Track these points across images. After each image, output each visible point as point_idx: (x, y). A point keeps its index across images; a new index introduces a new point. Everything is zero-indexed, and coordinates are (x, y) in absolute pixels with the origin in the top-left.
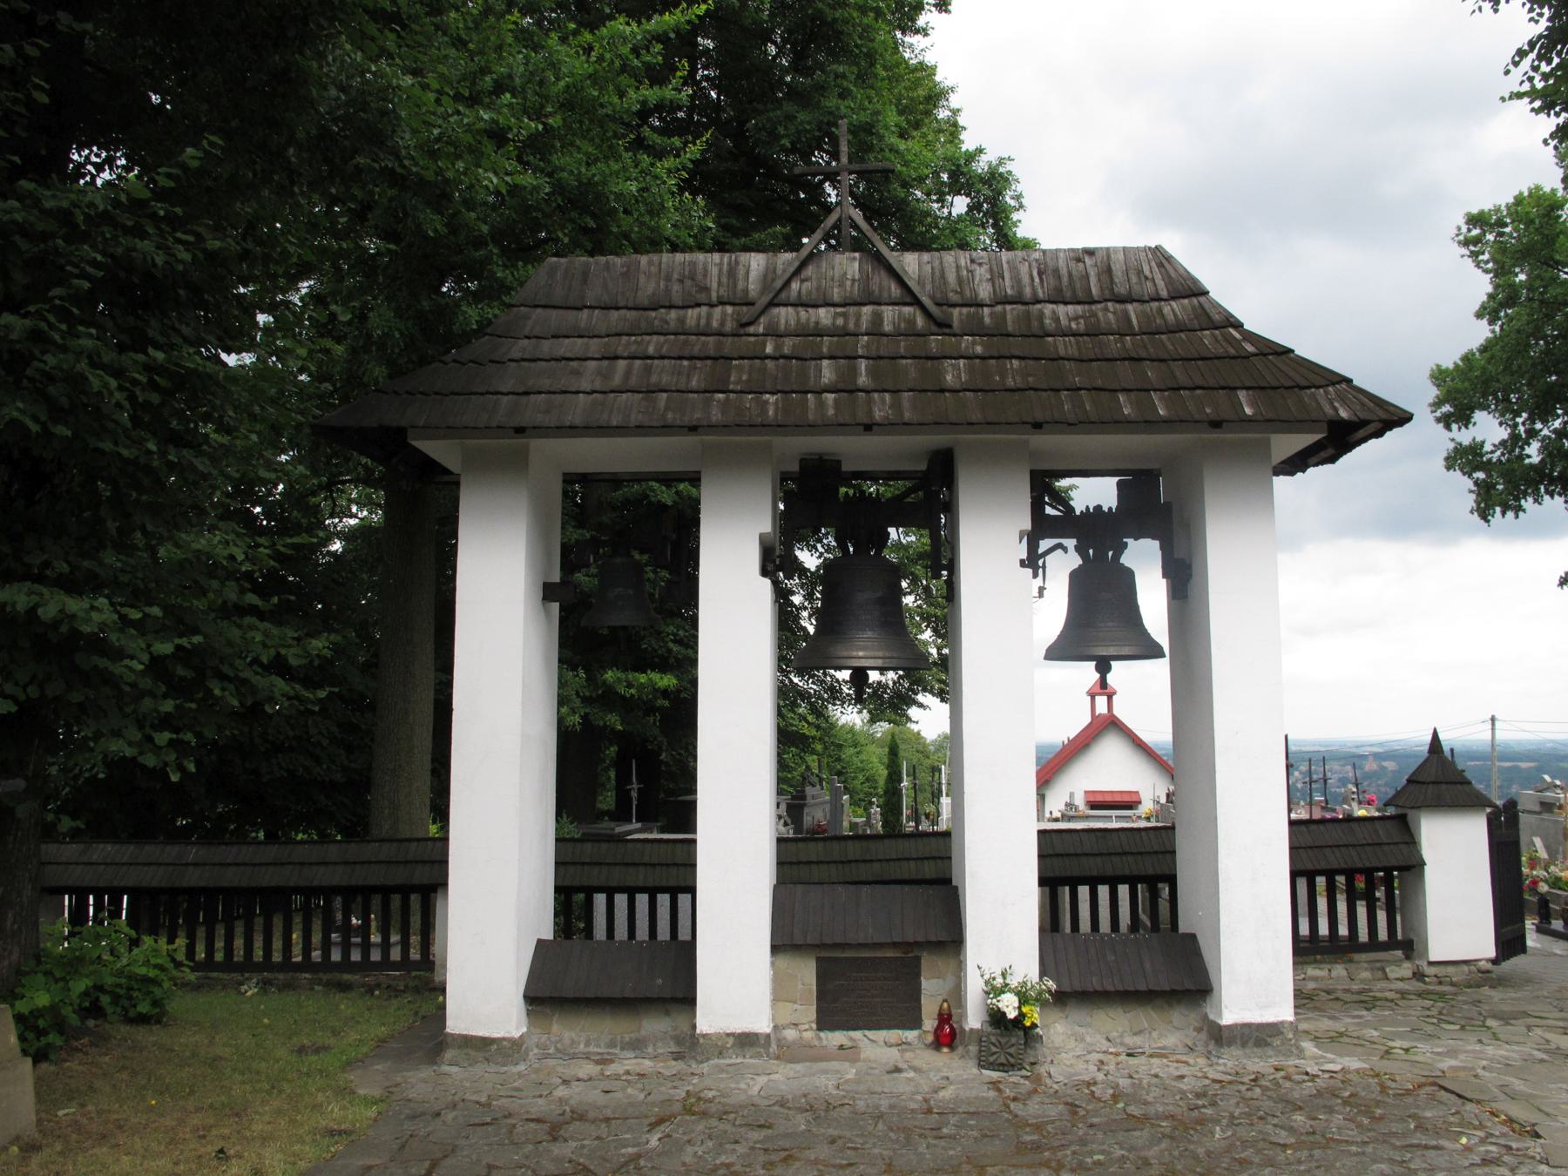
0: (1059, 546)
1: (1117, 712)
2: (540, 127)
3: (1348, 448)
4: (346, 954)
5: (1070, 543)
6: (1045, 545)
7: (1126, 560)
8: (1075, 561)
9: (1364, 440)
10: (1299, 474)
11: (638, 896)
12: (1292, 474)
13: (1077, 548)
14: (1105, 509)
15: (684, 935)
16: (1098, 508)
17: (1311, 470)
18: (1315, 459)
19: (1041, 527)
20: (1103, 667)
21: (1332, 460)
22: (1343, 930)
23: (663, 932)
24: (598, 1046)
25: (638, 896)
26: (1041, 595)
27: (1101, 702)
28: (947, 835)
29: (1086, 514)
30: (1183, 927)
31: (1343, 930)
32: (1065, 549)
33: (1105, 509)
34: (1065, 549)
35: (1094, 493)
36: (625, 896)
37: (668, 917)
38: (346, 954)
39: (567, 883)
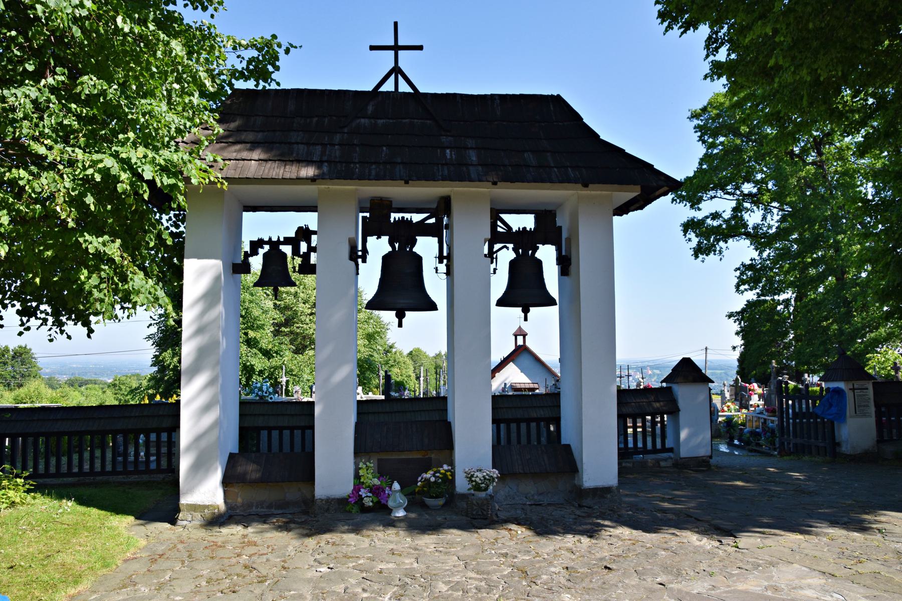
0: (505, 247)
1: (529, 344)
2: (720, 147)
3: (649, 201)
4: (158, 437)
5: (511, 246)
6: (497, 247)
7: (538, 255)
8: (512, 255)
9: (658, 197)
10: (625, 215)
11: (285, 432)
12: (621, 215)
13: (513, 249)
14: (528, 229)
15: (308, 450)
16: (524, 228)
17: (631, 213)
18: (633, 208)
19: (495, 238)
20: (526, 311)
21: (641, 208)
22: (640, 445)
23: (298, 448)
24: (262, 507)
25: (285, 432)
26: (495, 273)
27: (520, 339)
28: (445, 398)
29: (518, 232)
30: (564, 442)
31: (640, 445)
32: (508, 248)
33: (528, 229)
34: (508, 248)
35: (524, 222)
36: (277, 432)
37: (300, 443)
38: (158, 437)
39: (246, 425)
